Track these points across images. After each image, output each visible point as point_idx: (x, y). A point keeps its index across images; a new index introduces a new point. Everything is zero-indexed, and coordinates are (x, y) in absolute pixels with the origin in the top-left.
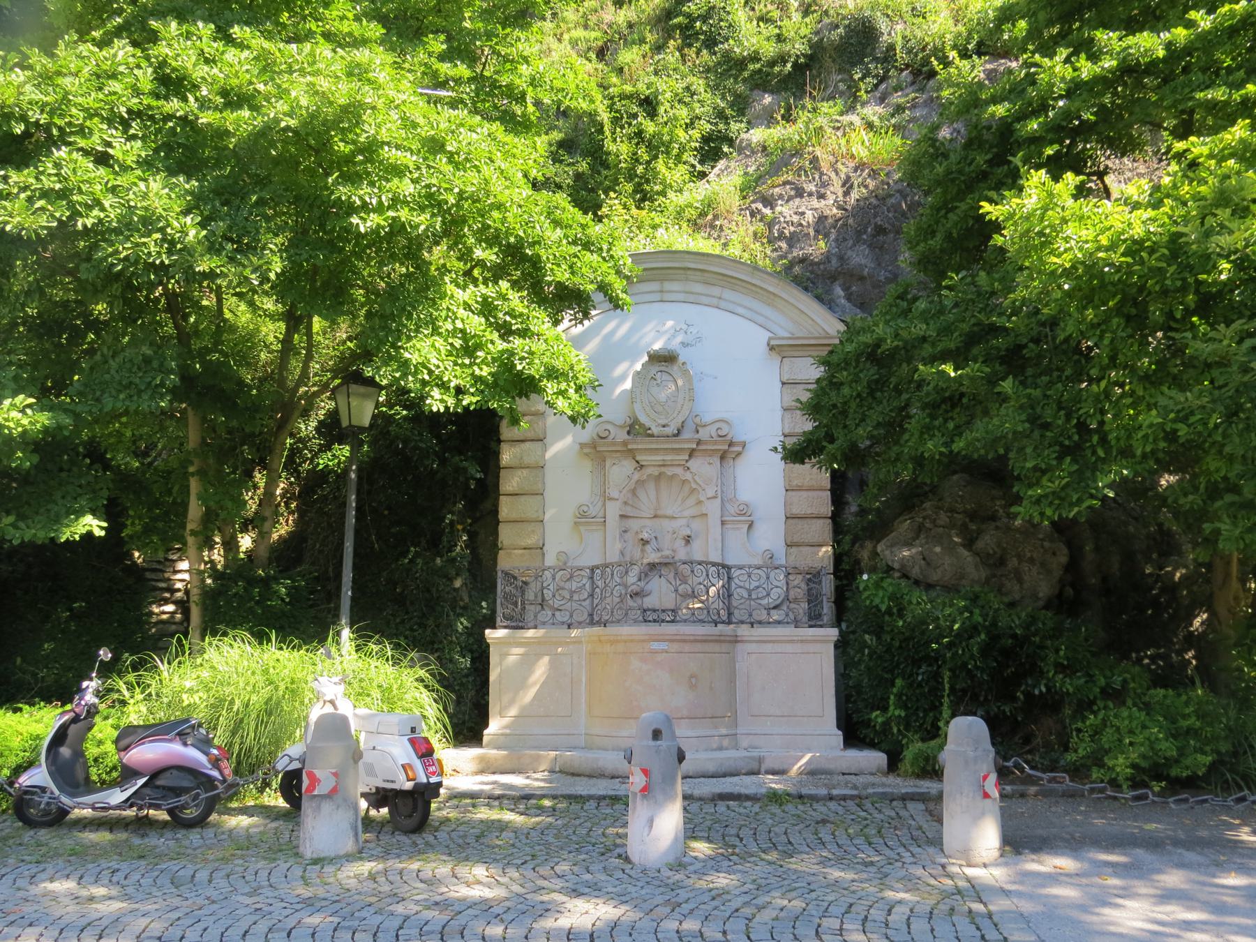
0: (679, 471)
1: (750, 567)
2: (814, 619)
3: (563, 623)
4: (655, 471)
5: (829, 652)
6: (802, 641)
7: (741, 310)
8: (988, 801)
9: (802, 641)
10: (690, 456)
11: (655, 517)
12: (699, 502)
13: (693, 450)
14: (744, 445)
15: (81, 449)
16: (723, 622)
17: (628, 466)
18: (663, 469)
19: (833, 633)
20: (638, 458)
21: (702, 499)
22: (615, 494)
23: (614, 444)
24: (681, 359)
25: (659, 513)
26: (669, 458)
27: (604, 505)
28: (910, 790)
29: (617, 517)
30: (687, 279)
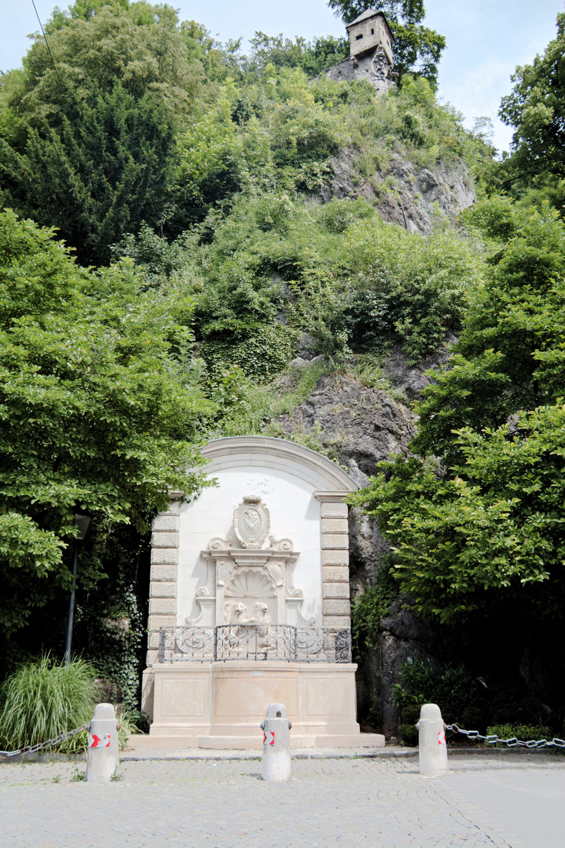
0: (260, 569)
1: (204, 627)
2: (341, 659)
3: (198, 660)
4: (246, 569)
5: (352, 678)
6: (337, 672)
7: (297, 473)
8: (273, 731)
9: (337, 672)
10: (268, 560)
11: (245, 597)
12: (272, 589)
13: (270, 557)
14: (298, 554)
15: (519, 117)
16: (292, 660)
17: (229, 566)
18: (251, 568)
19: (355, 666)
20: (236, 561)
21: (274, 586)
22: (221, 582)
23: (222, 552)
24: (263, 502)
25: (247, 594)
26: (255, 561)
27: (215, 589)
28: (383, 752)
29: (223, 597)
30: (266, 454)
